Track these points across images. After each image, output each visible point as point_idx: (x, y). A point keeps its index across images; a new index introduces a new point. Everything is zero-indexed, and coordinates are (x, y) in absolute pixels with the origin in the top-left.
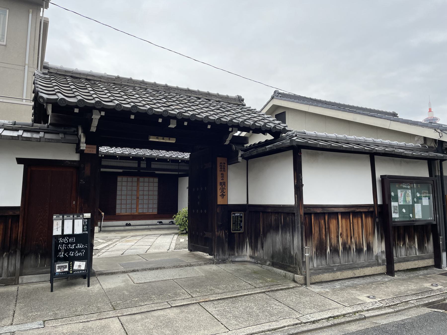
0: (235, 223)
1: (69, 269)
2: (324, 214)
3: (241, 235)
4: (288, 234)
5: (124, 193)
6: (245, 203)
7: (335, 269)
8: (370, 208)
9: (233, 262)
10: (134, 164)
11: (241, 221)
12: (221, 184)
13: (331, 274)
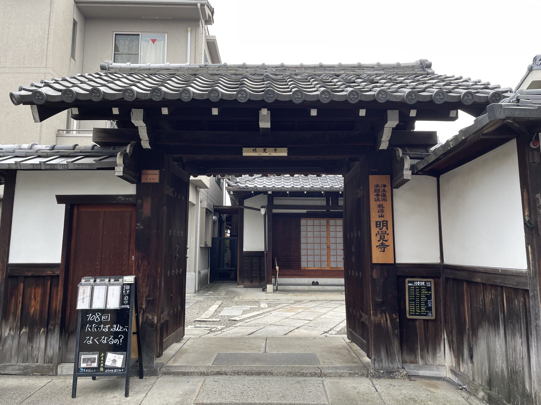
0: (415, 301)
1: (99, 364)
3: (430, 324)
4: (519, 340)
5: (310, 240)
6: (437, 261)
9: (410, 377)
10: (322, 202)
11: (429, 297)
12: (378, 224)
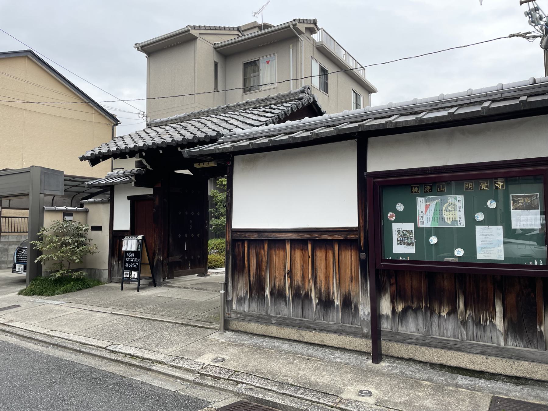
2: (262, 241)
7: (274, 322)
8: (349, 234)
13: (260, 326)
